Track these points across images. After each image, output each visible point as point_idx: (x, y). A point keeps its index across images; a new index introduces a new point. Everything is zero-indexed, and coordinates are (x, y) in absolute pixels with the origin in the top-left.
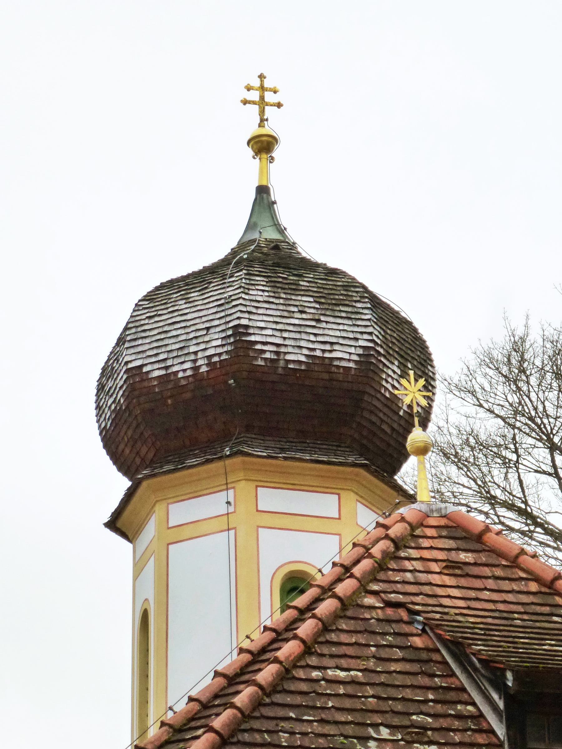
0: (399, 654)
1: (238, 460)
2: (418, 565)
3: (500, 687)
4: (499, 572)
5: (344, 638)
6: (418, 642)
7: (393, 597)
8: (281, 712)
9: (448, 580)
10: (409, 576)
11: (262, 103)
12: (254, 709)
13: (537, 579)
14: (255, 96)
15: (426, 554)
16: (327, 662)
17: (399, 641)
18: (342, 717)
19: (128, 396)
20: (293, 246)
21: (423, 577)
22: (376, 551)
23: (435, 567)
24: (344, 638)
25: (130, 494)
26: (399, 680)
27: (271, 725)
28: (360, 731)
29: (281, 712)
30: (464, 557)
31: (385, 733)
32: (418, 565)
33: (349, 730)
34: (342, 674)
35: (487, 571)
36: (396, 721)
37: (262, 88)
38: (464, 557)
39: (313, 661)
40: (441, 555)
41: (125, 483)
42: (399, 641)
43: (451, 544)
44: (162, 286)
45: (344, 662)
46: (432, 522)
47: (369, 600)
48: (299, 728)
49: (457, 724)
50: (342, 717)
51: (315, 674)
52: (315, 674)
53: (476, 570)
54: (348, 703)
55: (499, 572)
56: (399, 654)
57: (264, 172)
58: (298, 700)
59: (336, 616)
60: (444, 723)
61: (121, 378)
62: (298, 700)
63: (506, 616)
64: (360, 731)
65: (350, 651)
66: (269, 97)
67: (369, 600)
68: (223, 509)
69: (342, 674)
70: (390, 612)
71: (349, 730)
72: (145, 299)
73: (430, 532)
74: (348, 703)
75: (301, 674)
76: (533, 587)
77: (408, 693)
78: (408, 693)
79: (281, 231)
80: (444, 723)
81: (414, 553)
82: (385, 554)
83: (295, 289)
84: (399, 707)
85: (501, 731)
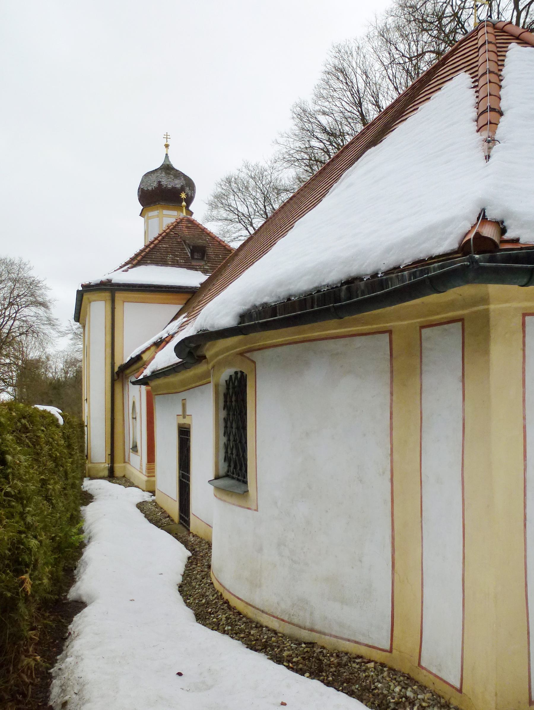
0: (176, 242)
1: (159, 205)
2: (181, 227)
3: (190, 248)
4: (195, 228)
5: (166, 240)
6: (179, 240)
7: (176, 232)
8: (154, 253)
9: (186, 229)
10: (179, 229)
11: (167, 138)
12: (149, 252)
13: (201, 229)
14: (166, 137)
15: (183, 225)
16: (163, 244)
17: (176, 240)
18: (164, 253)
19: (141, 193)
20: (171, 165)
21: (182, 229)
22: (174, 224)
23: (184, 227)
24: (166, 240)
25: (143, 209)
26: (175, 247)
27: (151, 255)
28: (166, 255)
29: (154, 253)
30: (189, 225)
31: (171, 256)
32: (181, 227)
33: (165, 255)
34: (165, 246)
35: (193, 228)
36: (173, 254)
37: (167, 135)
38: (189, 225)
39: (160, 244)
40: (185, 225)
41: (142, 207)
42: (176, 240)
43: (187, 223)
44: (148, 173)
45: (165, 244)
46: (185, 219)
47: (172, 233)
48: (156, 255)
49: (183, 254)
50: (164, 253)
51: (161, 246)
52: (161, 246)
53: (191, 227)
54: (165, 251)
55: (195, 228)
56: (176, 242)
57: (167, 151)
58: (157, 250)
59: (166, 236)
60: (181, 254)
61: (140, 190)
62: (157, 250)
63: (194, 236)
64: (166, 255)
65: (167, 242)
66: (168, 137)
67: (172, 233)
68: (157, 214)
69: (165, 246)
70: (175, 235)
71: (165, 255)
72: (145, 175)
73: (184, 221)
74: (165, 251)
75: (158, 246)
76: (200, 230)
77: (176, 249)
78: (176, 249)
79: (170, 162)
80: (181, 254)
81: (181, 224)
82: (176, 225)
83: (169, 174)
84: (174, 251)
85: (190, 255)
